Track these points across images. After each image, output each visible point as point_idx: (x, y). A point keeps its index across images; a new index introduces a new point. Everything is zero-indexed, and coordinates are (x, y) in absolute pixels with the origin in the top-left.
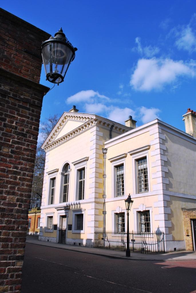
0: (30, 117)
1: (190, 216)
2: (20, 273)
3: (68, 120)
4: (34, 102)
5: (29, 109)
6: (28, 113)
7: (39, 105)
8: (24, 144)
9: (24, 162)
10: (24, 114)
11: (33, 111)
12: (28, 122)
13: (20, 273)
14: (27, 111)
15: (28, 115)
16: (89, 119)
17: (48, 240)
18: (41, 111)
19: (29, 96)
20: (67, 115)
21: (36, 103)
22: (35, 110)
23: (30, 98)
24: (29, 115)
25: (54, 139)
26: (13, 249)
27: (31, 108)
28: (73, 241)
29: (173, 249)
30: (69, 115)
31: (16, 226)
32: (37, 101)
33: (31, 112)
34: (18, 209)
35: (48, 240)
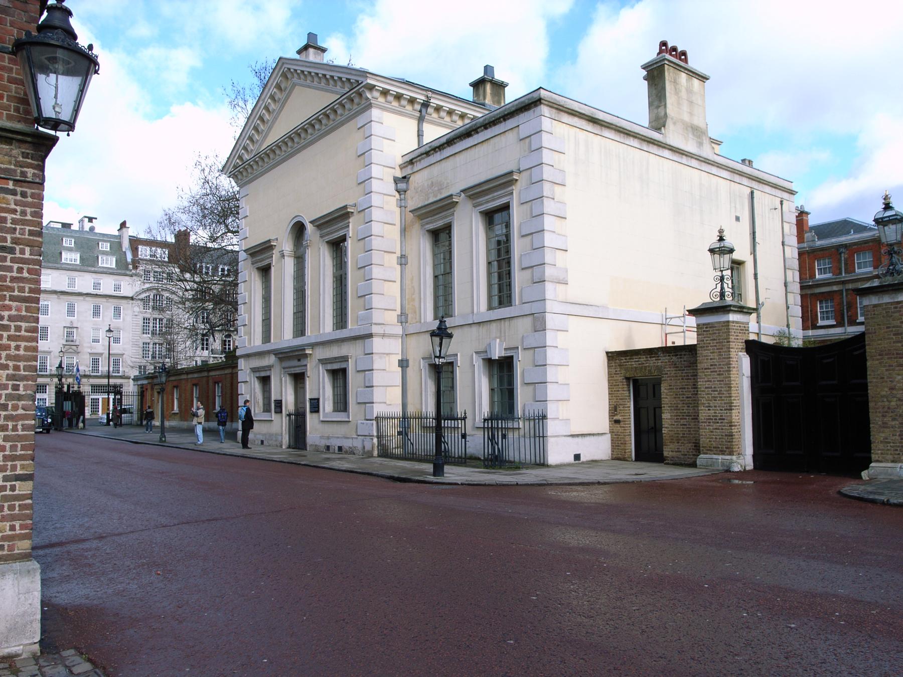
0: (18, 208)
1: (627, 370)
2: (30, 501)
3: (294, 85)
4: (24, 174)
5: (14, 193)
6: (12, 202)
7: (37, 180)
8: (12, 267)
9: (14, 304)
10: (4, 206)
11: (24, 195)
12: (14, 221)
13: (30, 501)
14: (10, 197)
15: (13, 206)
16: (351, 83)
17: (262, 442)
18: (44, 193)
19: (10, 163)
20: (289, 69)
21: (29, 175)
22: (29, 191)
23: (13, 167)
24: (15, 205)
25: (261, 145)
26: (9, 463)
27: (19, 189)
28: (323, 443)
29: (571, 459)
30: (296, 68)
31: (10, 424)
32: (30, 172)
33: (19, 197)
34: (10, 394)
35: (262, 442)
